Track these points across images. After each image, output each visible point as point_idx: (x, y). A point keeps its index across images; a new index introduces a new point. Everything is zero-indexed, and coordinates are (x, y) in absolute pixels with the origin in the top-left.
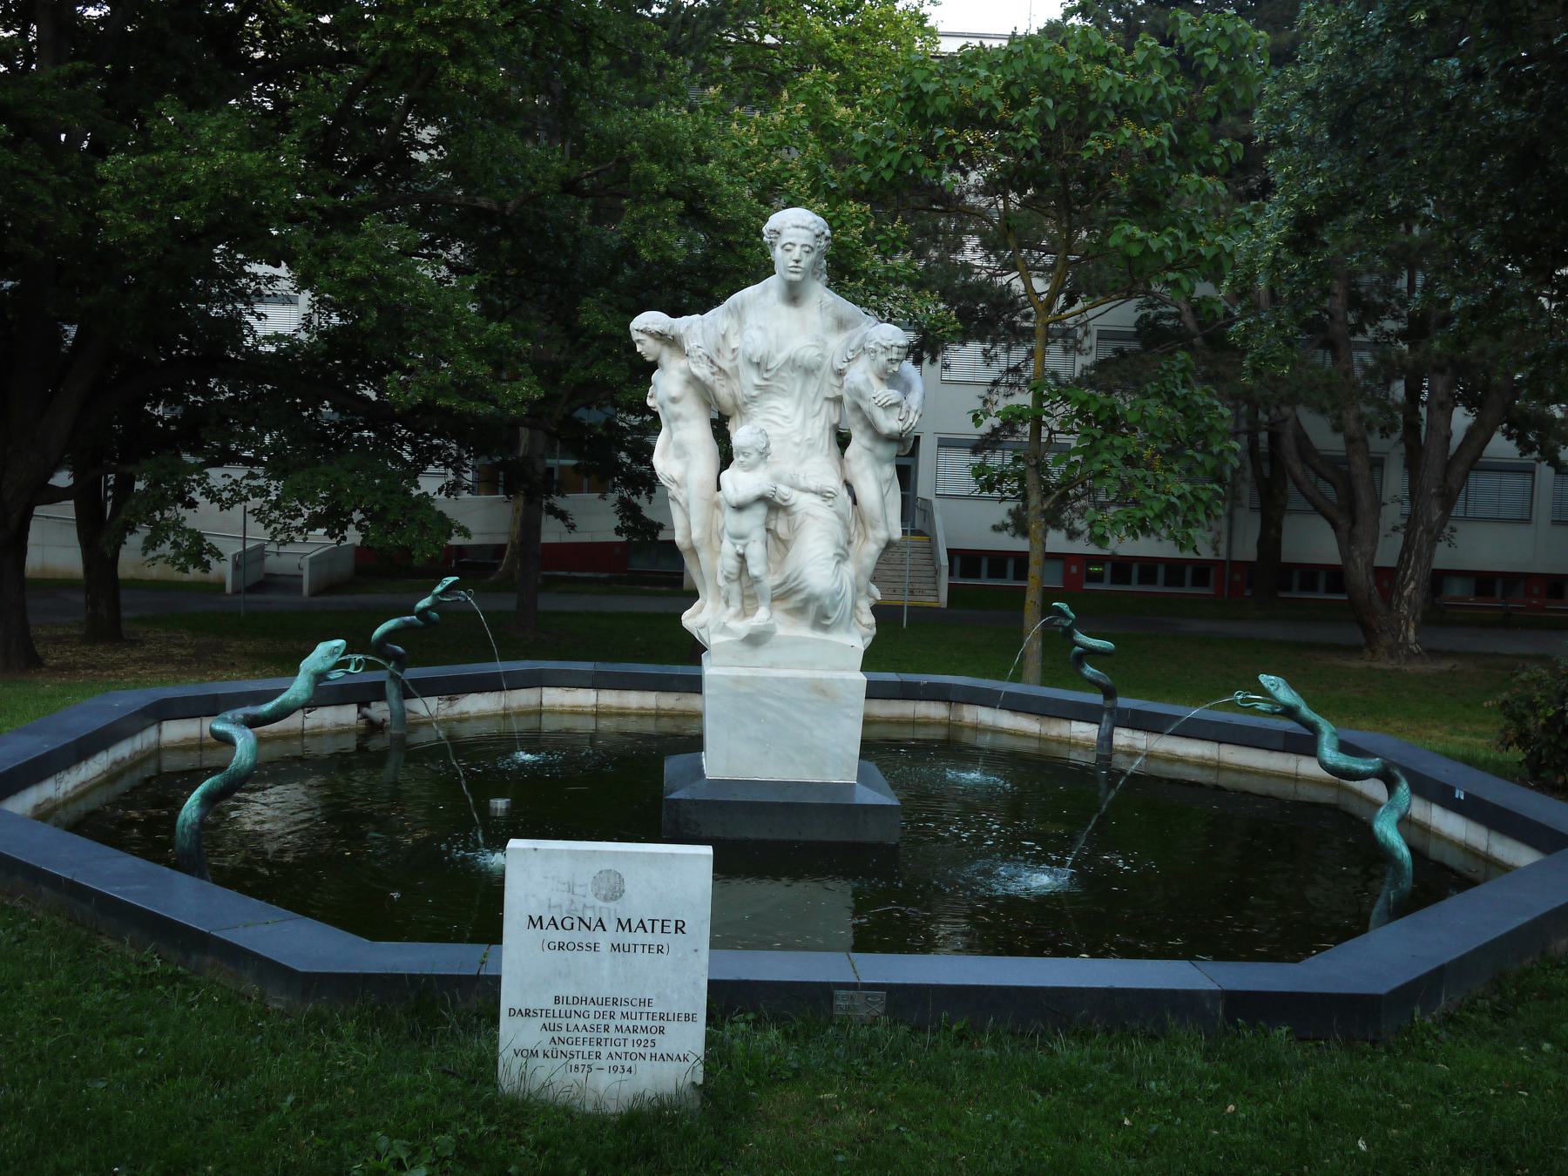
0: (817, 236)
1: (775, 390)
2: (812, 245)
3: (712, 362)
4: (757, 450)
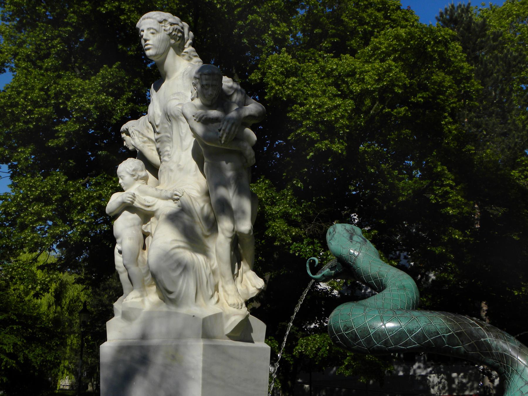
0: (160, 22)
1: (165, 139)
2: (155, 27)
3: (142, 134)
4: (128, 173)
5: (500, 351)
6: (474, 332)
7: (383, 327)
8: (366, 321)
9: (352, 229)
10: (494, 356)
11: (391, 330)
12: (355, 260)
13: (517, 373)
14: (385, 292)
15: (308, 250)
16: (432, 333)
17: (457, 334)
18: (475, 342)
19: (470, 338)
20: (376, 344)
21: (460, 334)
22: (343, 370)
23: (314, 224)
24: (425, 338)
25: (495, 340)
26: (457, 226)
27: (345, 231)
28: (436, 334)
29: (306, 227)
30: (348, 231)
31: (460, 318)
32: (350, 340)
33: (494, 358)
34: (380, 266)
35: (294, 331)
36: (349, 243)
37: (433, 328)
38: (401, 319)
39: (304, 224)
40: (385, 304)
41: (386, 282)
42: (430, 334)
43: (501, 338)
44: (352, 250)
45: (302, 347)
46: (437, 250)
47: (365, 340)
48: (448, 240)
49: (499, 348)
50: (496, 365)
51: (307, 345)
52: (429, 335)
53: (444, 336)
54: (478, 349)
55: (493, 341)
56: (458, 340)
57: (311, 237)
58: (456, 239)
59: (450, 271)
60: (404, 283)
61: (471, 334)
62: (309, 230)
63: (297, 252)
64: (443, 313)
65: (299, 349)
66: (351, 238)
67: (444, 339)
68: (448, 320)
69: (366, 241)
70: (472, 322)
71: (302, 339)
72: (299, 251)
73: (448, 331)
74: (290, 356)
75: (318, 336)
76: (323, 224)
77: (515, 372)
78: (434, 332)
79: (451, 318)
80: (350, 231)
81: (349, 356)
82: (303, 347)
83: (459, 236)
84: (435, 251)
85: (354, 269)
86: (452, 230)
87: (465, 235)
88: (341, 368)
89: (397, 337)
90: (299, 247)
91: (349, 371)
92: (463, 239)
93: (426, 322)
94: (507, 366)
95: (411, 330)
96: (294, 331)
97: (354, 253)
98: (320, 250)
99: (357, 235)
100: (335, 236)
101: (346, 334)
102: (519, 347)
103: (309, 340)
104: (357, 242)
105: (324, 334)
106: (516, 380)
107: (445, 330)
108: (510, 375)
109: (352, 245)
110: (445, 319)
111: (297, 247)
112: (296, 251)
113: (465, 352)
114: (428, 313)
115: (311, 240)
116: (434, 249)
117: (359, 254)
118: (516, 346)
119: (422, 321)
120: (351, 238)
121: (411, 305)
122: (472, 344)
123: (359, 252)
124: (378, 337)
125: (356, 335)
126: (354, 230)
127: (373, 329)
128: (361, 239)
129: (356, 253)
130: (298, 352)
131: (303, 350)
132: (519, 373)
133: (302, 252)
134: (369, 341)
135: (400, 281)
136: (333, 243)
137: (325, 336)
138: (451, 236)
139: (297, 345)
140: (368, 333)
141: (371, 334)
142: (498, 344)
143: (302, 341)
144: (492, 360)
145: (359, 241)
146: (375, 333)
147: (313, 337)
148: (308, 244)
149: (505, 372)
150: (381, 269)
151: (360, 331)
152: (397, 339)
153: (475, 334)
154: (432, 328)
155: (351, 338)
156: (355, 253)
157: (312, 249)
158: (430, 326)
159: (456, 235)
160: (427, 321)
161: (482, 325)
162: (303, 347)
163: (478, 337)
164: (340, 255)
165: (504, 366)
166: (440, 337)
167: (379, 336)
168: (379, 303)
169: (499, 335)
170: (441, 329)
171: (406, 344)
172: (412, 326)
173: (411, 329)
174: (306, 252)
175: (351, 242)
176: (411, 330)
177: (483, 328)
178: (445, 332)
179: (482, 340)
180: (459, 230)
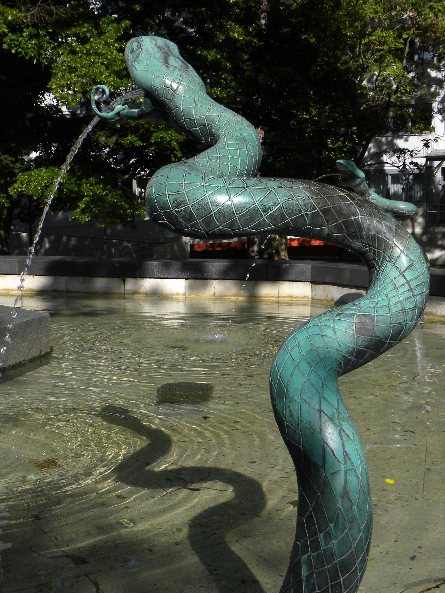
5: (373, 233)
6: (344, 208)
7: (229, 203)
8: (207, 195)
9: (167, 45)
10: (364, 239)
11: (239, 208)
12: (173, 95)
13: (391, 261)
14: (218, 146)
15: (30, 46)
16: (292, 212)
17: (323, 211)
18: (342, 221)
19: (338, 216)
20: (218, 227)
21: (326, 212)
22: (78, 215)
23: (39, 6)
24: (283, 217)
25: (369, 219)
26: (239, 21)
27: (156, 49)
28: (297, 212)
29: (28, 10)
30: (161, 50)
31: (327, 188)
32: (181, 220)
33: (363, 241)
34: (208, 107)
35: (9, 162)
36: (164, 68)
37: (295, 203)
38: (255, 192)
39: (24, 5)
40: (221, 166)
41: (218, 130)
42: (291, 212)
43: (375, 216)
44: (168, 79)
45: (23, 185)
46: (210, 55)
47: (203, 221)
48: (224, 40)
49: (372, 228)
50: (364, 250)
51: (29, 182)
52: (289, 213)
53: (307, 215)
54: (345, 231)
55: (365, 219)
56: (323, 219)
57: (34, 25)
58: (234, 37)
59: (223, 85)
60: (244, 134)
61: (340, 212)
62: (33, 15)
63: (13, 48)
64: (307, 183)
65: (19, 187)
66: (166, 61)
67: (306, 218)
68: (314, 193)
69: (187, 67)
70: (342, 194)
71: (22, 175)
72: (16, 46)
73: (312, 207)
74: (4, 197)
75: (44, 171)
76: (53, 8)
77: (388, 259)
78: (296, 210)
79: (317, 189)
80: (164, 48)
81: (87, 196)
82: (23, 185)
83: (239, 35)
84: (207, 57)
85: (170, 110)
86: (231, 25)
87: (248, 33)
88: (76, 213)
89: (247, 217)
90: (18, 41)
91: (86, 215)
92: (244, 39)
93: (286, 196)
94: (378, 252)
95: (267, 208)
96: (9, 162)
97: (171, 86)
98: (48, 47)
99: (174, 56)
100: (142, 55)
101: (175, 211)
102: (396, 226)
103: (31, 175)
104: (175, 67)
105: (53, 168)
106: (388, 269)
107: (309, 206)
108: (381, 263)
109: (168, 72)
110: (310, 191)
111: (14, 40)
112: (13, 45)
113: (328, 234)
114: (287, 182)
115: (34, 32)
116: (205, 53)
117: (177, 88)
118: (392, 226)
119: (281, 195)
120: (166, 61)
121: (253, 166)
122: (340, 223)
123: (179, 84)
124: (222, 217)
125: (191, 214)
126: (169, 48)
127: (216, 206)
128: (181, 63)
129: (175, 86)
130: (17, 191)
131: (24, 189)
132: (394, 261)
133: (22, 48)
134: (209, 221)
135: (239, 130)
136: (138, 67)
137: (53, 171)
138: (229, 33)
139: (15, 182)
140: (209, 212)
141: (213, 213)
142: (371, 224)
143: (21, 177)
144: (360, 244)
145: (177, 65)
146: (218, 212)
147: (38, 172)
148: (31, 37)
149: (374, 259)
150: (212, 111)
151: (196, 208)
152: (247, 220)
153: (345, 210)
154: (294, 204)
155: (184, 218)
156: (173, 86)
157: (35, 44)
158: (292, 201)
159: (234, 33)
160: (288, 194)
161: (353, 199)
162: (23, 185)
163: (348, 215)
164: (151, 88)
165: (374, 251)
166: (303, 215)
167: (224, 216)
168: (214, 164)
169: (373, 211)
170: (304, 205)
171: (258, 225)
172: (268, 202)
173: (267, 206)
174: (28, 48)
175: (167, 67)
176: (267, 208)
177: (354, 202)
178: (309, 210)
179: (353, 218)
180: (240, 26)
